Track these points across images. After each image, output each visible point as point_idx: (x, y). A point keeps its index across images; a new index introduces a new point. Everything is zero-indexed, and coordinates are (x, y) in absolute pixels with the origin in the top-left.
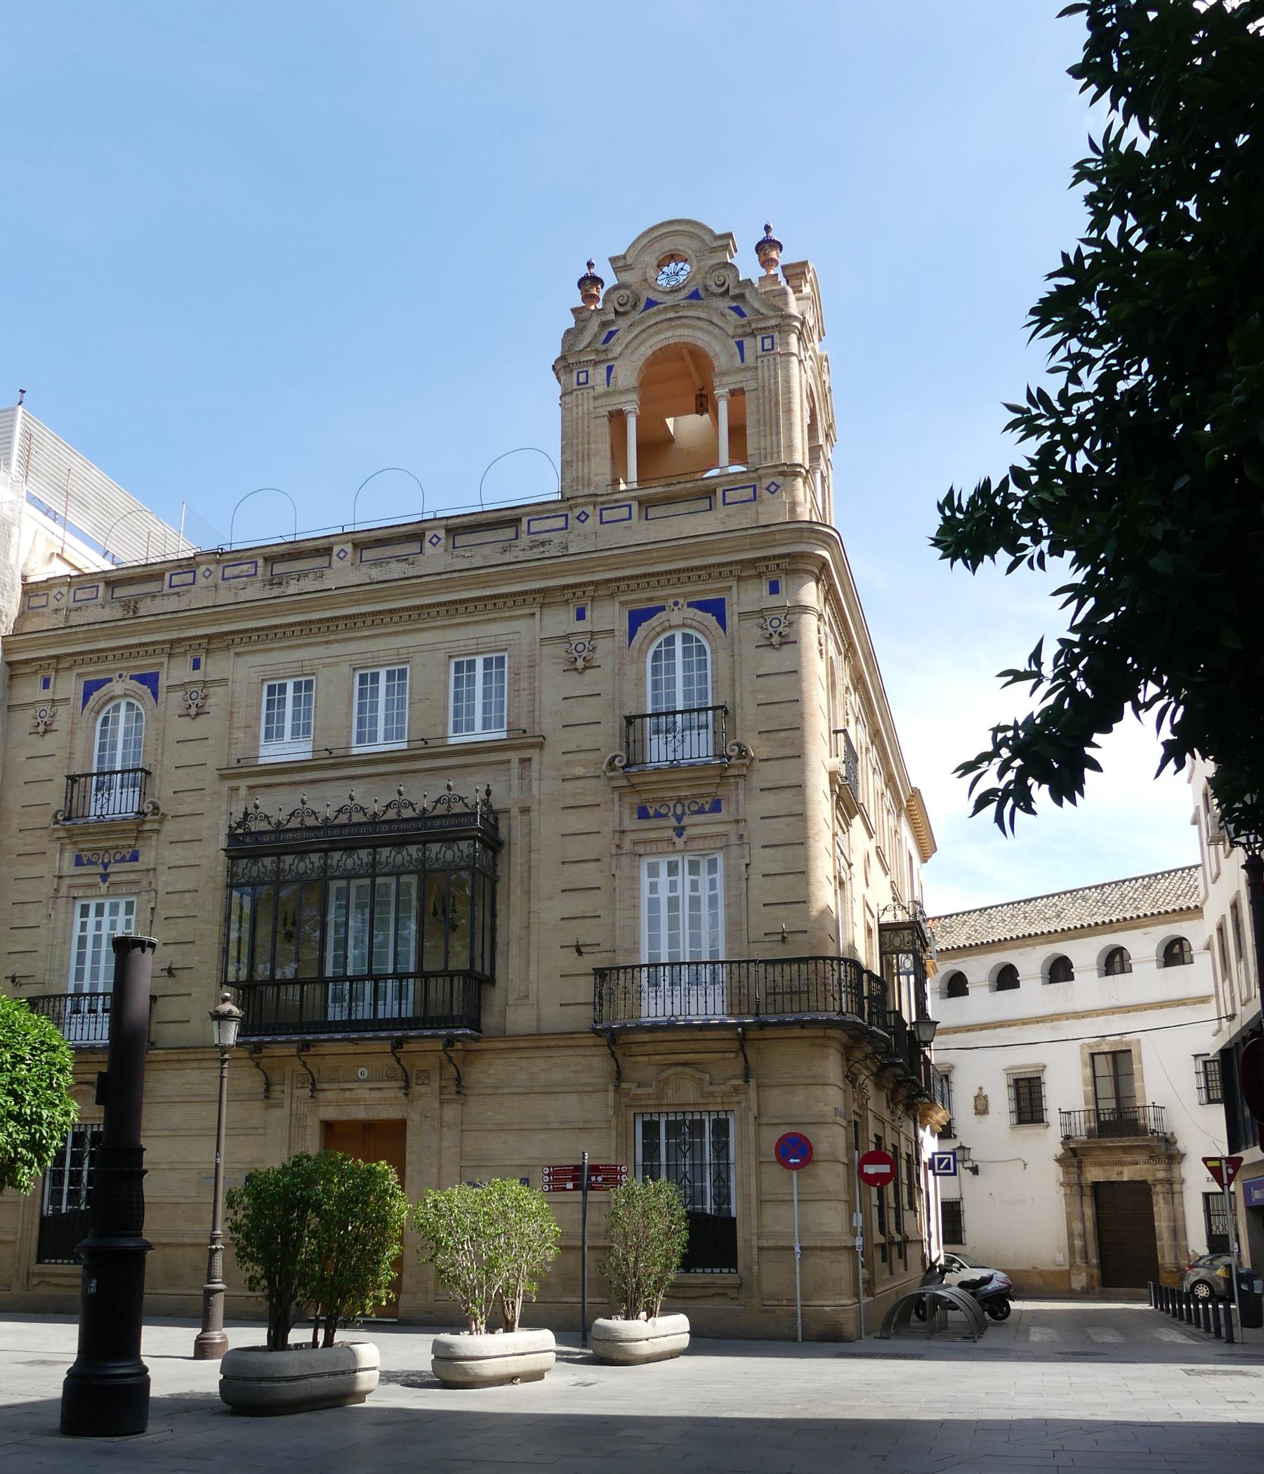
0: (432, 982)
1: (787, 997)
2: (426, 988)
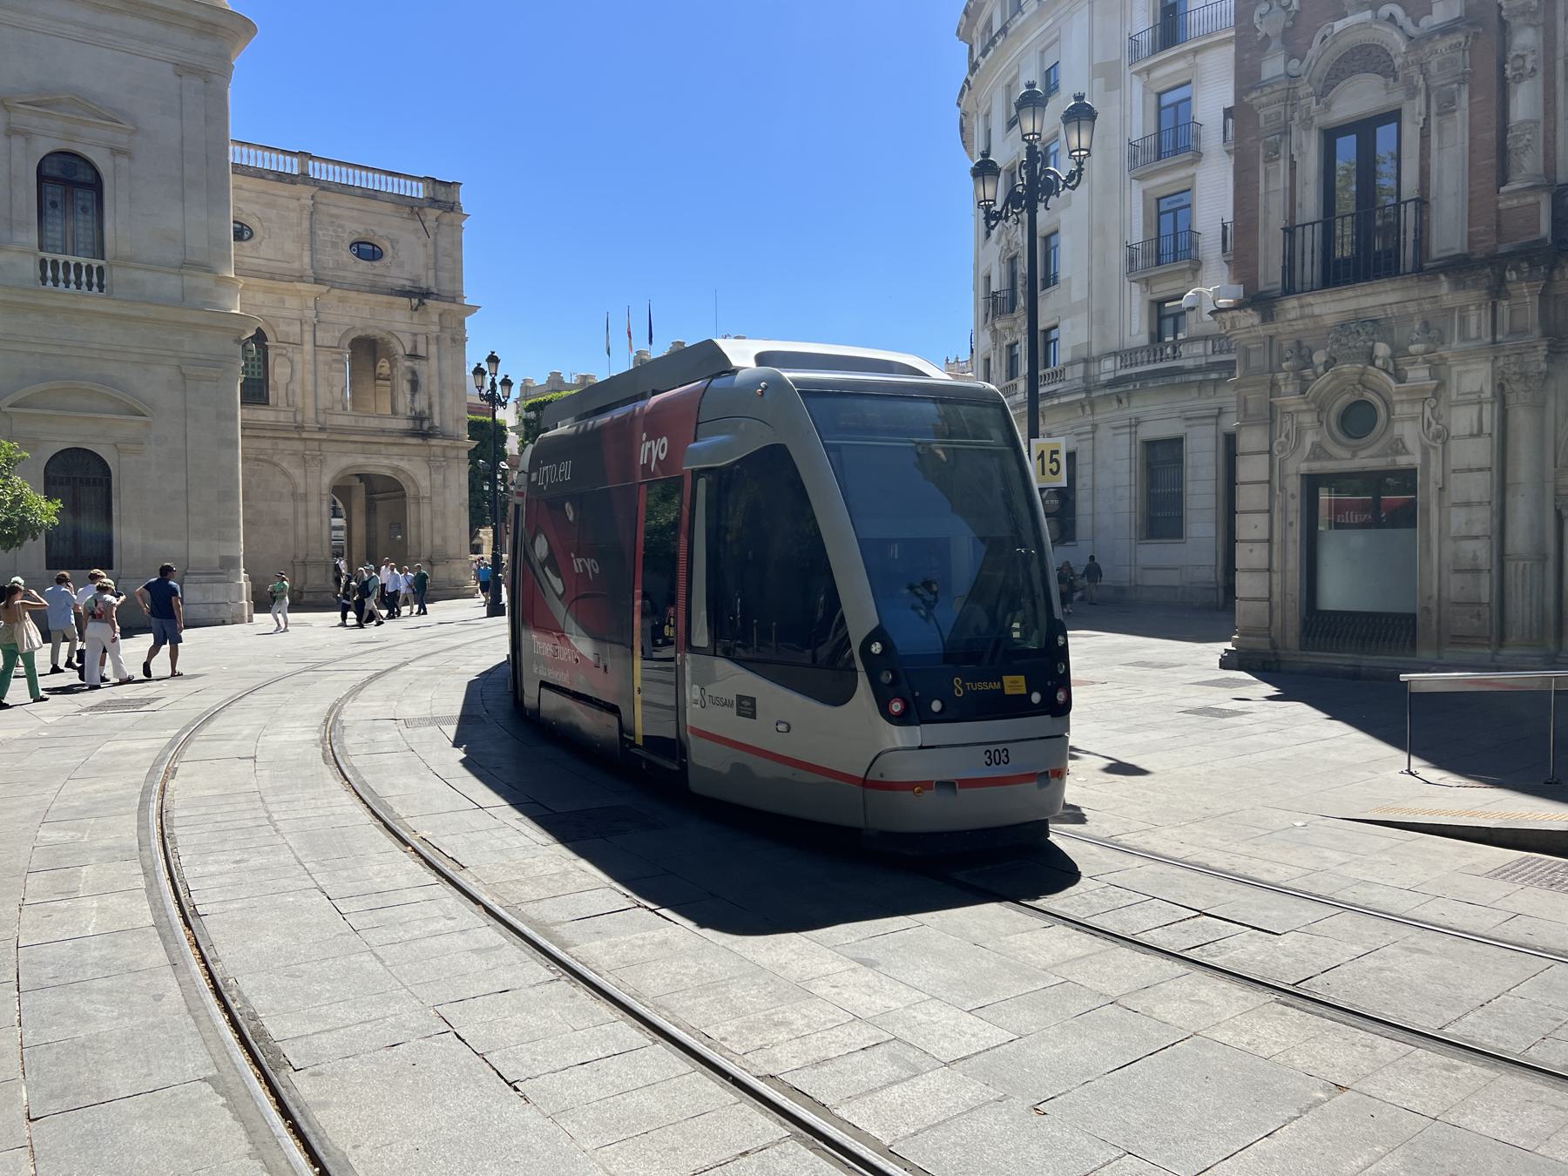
0: (1270, 190)
1: (1091, 436)
2: (1263, 482)
